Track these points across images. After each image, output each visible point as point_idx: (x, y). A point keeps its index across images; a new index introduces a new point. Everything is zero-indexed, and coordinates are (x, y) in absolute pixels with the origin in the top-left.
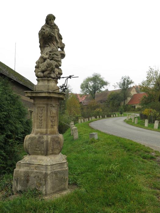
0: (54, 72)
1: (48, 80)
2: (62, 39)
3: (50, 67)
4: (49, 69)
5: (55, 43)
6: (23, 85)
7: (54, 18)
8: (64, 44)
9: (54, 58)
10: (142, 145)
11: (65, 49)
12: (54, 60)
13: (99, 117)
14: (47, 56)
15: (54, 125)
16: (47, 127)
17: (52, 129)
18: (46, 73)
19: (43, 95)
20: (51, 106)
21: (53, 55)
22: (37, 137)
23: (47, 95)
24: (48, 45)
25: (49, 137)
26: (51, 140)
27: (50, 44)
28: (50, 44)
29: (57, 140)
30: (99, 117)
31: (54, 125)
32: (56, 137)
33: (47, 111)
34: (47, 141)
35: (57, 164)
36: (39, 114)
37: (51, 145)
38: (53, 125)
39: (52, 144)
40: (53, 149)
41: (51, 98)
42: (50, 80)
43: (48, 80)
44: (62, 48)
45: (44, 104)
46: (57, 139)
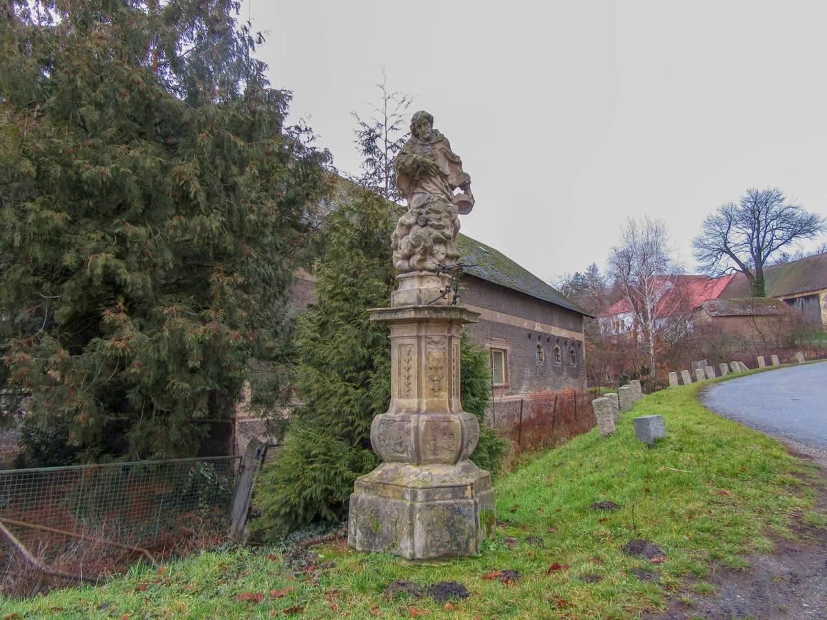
0: (432, 255)
1: (421, 277)
2: (459, 163)
3: (418, 246)
4: (418, 249)
5: (438, 180)
6: (494, 284)
7: (429, 119)
8: (466, 175)
9: (431, 221)
10: (368, 430)
11: (473, 188)
12: (432, 226)
13: (769, 362)
14: (412, 220)
15: (439, 389)
16: (419, 395)
17: (436, 399)
18: (414, 261)
19: (407, 315)
20: (429, 340)
21: (427, 213)
22: (398, 419)
23: (412, 315)
24: (420, 190)
25: (424, 418)
26: (426, 427)
27: (424, 185)
28: (424, 185)
29: (447, 428)
30: (769, 362)
31: (439, 389)
32: (444, 418)
33: (419, 354)
34: (417, 429)
35: (444, 487)
36: (403, 362)
37: (429, 438)
38: (436, 389)
39: (432, 435)
40: (435, 449)
41: (428, 322)
42: (426, 275)
43: (421, 277)
44: (465, 186)
45: (412, 337)
46: (445, 424)
